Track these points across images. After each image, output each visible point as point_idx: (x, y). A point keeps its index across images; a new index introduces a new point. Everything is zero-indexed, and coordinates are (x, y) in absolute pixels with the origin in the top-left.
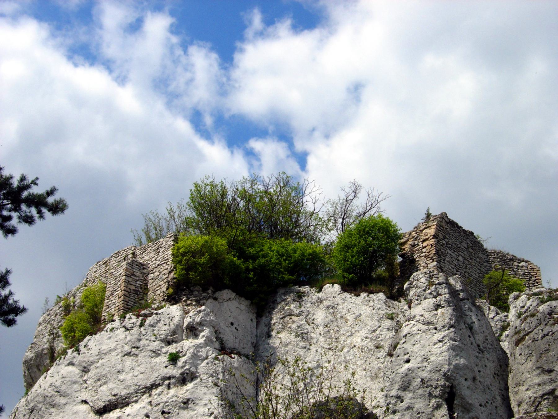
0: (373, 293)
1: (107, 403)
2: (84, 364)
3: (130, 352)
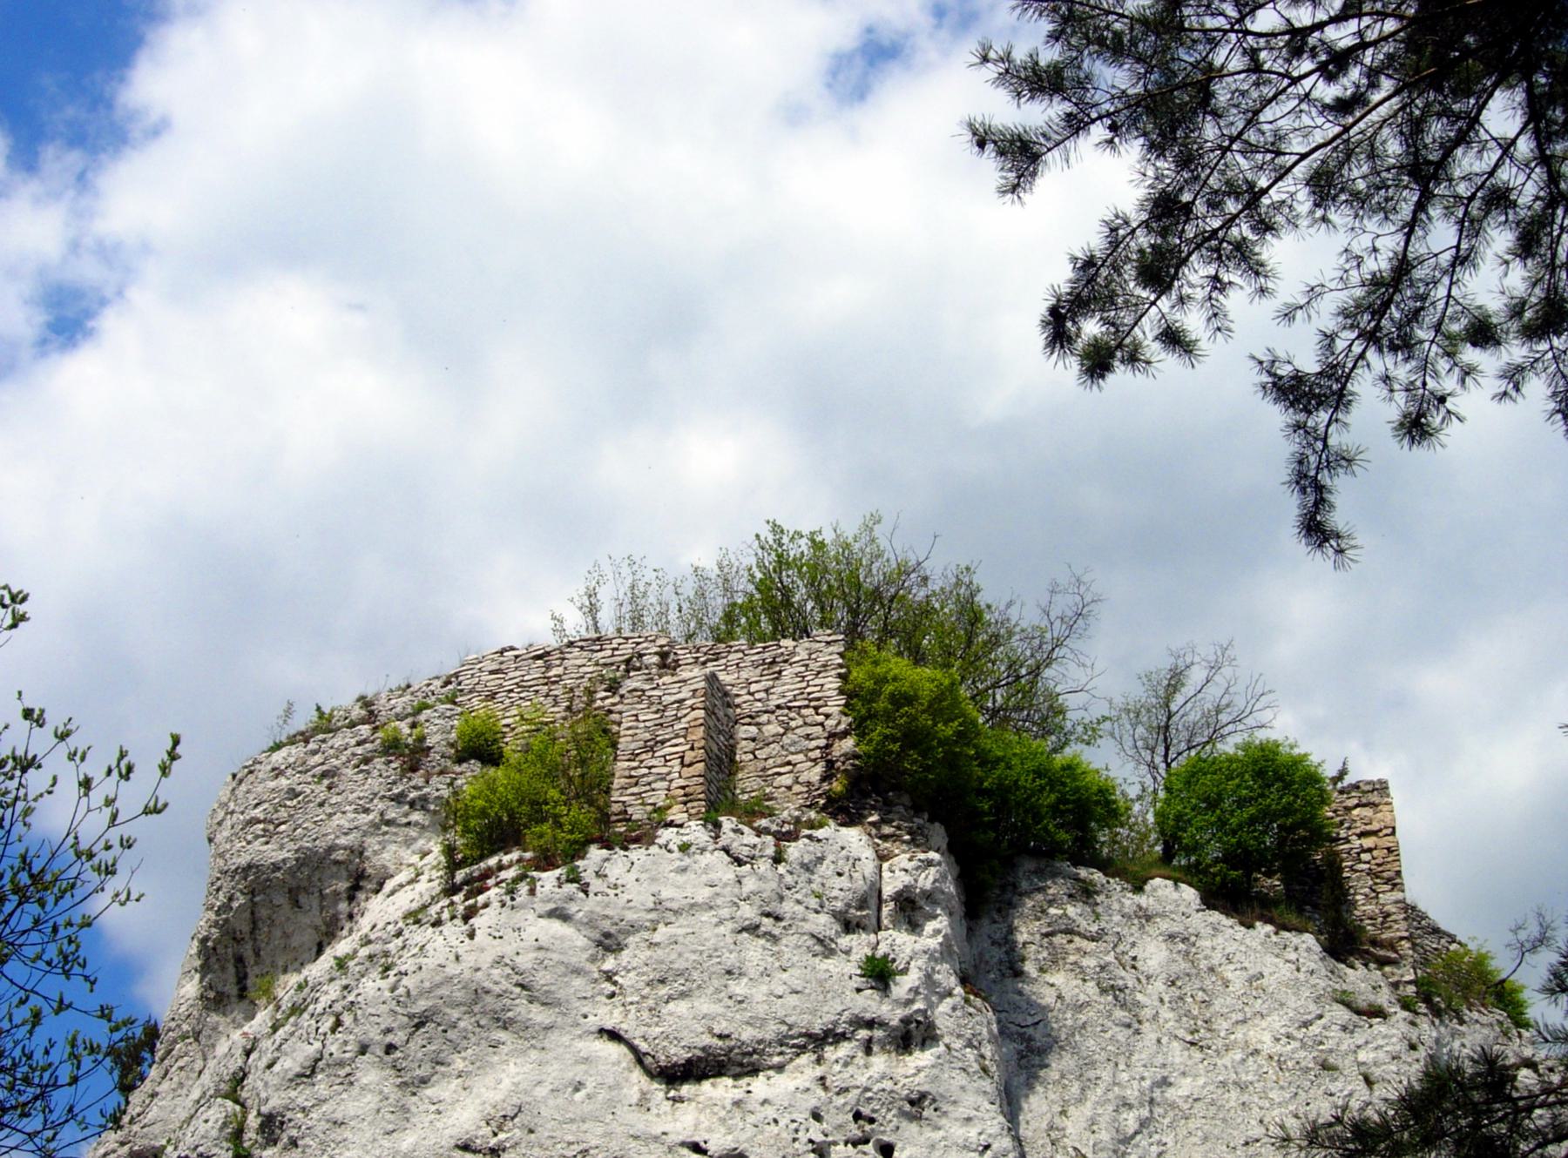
0: (1289, 930)
1: (699, 1053)
2: (606, 926)
3: (757, 927)
